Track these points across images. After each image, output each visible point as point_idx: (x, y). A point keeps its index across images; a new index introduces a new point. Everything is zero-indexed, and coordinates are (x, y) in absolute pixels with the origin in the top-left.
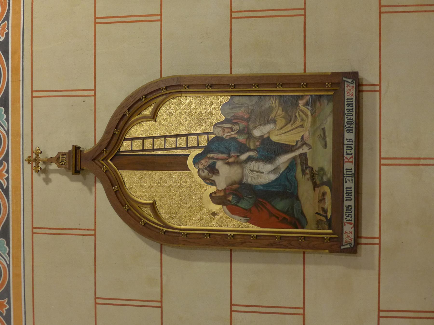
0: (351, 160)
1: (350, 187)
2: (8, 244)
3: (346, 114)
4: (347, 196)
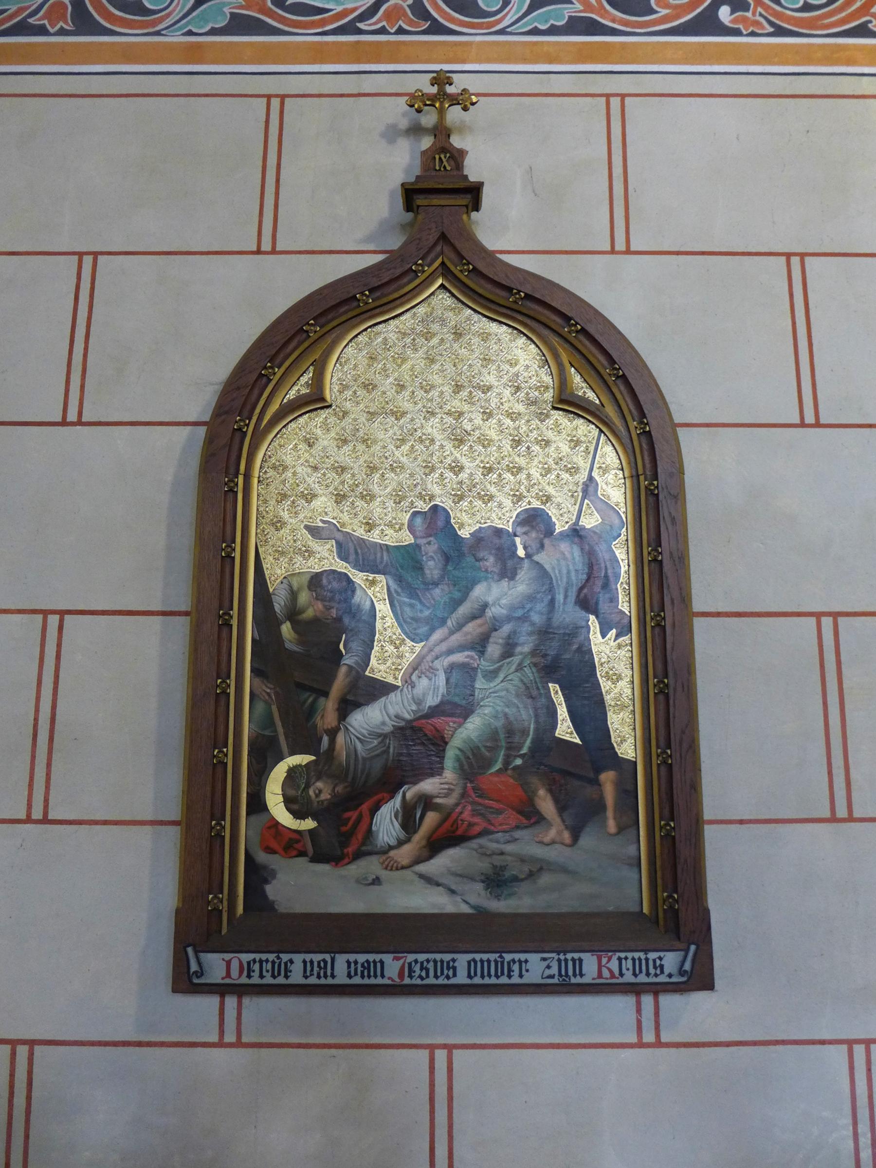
0: (606, 973)
1: (583, 973)
2: (213, 32)
3: (278, 958)
4: (316, 964)
